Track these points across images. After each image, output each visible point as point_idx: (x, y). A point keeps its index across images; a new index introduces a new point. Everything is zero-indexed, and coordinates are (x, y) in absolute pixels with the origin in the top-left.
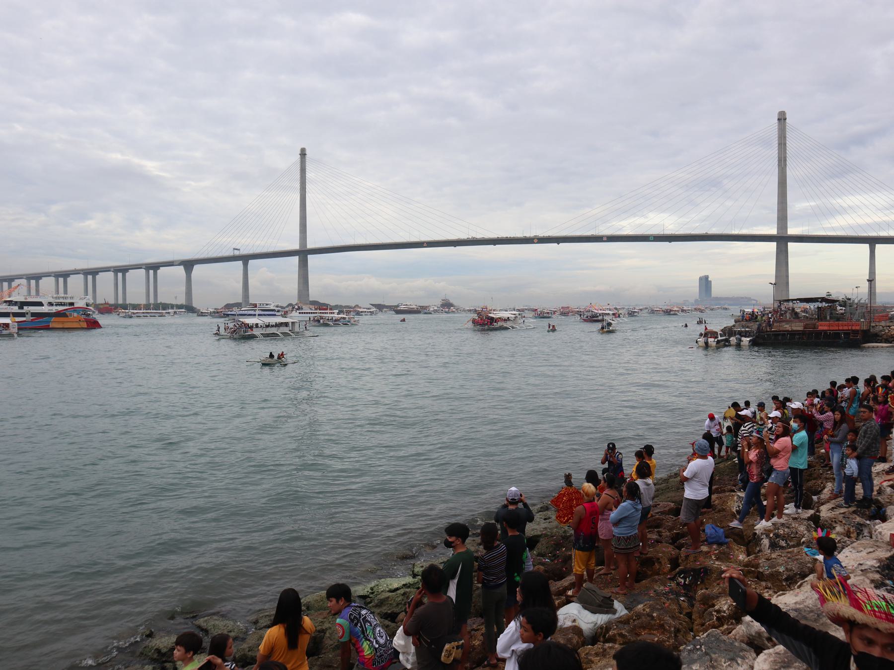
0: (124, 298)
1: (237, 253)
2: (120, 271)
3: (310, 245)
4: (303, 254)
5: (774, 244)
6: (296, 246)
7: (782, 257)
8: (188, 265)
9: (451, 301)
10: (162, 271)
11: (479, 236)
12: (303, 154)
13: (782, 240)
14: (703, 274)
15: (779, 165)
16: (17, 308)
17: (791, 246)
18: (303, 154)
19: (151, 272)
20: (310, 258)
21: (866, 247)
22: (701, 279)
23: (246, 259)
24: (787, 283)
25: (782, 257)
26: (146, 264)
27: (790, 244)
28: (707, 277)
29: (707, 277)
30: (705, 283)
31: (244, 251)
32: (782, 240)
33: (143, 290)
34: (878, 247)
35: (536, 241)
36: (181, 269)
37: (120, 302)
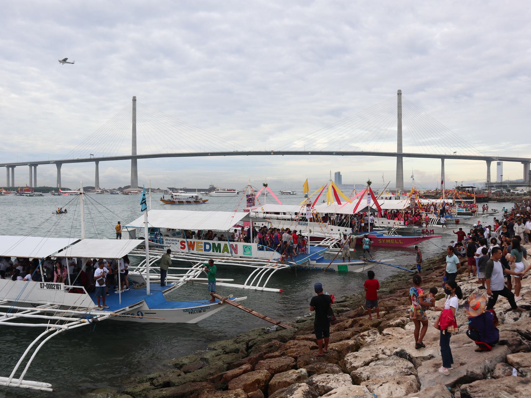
0: (13, 183)
1: (92, 157)
2: (10, 166)
3: (138, 153)
4: (134, 158)
5: (130, 160)
6: (130, 154)
7: (134, 165)
8: (59, 164)
9: (215, 186)
10: (39, 167)
11: (240, 150)
12: (134, 100)
13: (400, 156)
14: (337, 171)
15: (398, 117)
16: (464, 210)
17: (138, 160)
18: (134, 100)
19: (10, 169)
20: (138, 160)
21: (440, 160)
22: (336, 174)
23: (97, 160)
24: (403, 178)
25: (134, 165)
26: (30, 163)
27: (138, 160)
28: (339, 173)
29: (339, 173)
30: (338, 176)
31: (96, 156)
32: (134, 158)
33: (5, 180)
34: (445, 160)
35: (272, 153)
36: (55, 166)
37: (11, 186)
